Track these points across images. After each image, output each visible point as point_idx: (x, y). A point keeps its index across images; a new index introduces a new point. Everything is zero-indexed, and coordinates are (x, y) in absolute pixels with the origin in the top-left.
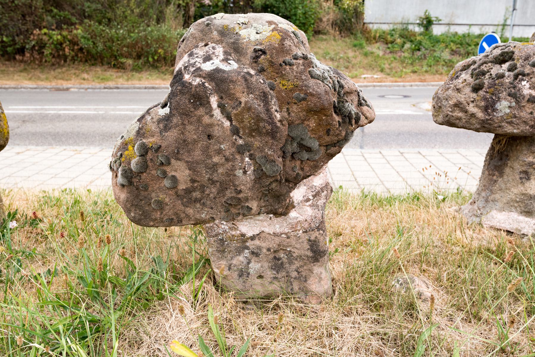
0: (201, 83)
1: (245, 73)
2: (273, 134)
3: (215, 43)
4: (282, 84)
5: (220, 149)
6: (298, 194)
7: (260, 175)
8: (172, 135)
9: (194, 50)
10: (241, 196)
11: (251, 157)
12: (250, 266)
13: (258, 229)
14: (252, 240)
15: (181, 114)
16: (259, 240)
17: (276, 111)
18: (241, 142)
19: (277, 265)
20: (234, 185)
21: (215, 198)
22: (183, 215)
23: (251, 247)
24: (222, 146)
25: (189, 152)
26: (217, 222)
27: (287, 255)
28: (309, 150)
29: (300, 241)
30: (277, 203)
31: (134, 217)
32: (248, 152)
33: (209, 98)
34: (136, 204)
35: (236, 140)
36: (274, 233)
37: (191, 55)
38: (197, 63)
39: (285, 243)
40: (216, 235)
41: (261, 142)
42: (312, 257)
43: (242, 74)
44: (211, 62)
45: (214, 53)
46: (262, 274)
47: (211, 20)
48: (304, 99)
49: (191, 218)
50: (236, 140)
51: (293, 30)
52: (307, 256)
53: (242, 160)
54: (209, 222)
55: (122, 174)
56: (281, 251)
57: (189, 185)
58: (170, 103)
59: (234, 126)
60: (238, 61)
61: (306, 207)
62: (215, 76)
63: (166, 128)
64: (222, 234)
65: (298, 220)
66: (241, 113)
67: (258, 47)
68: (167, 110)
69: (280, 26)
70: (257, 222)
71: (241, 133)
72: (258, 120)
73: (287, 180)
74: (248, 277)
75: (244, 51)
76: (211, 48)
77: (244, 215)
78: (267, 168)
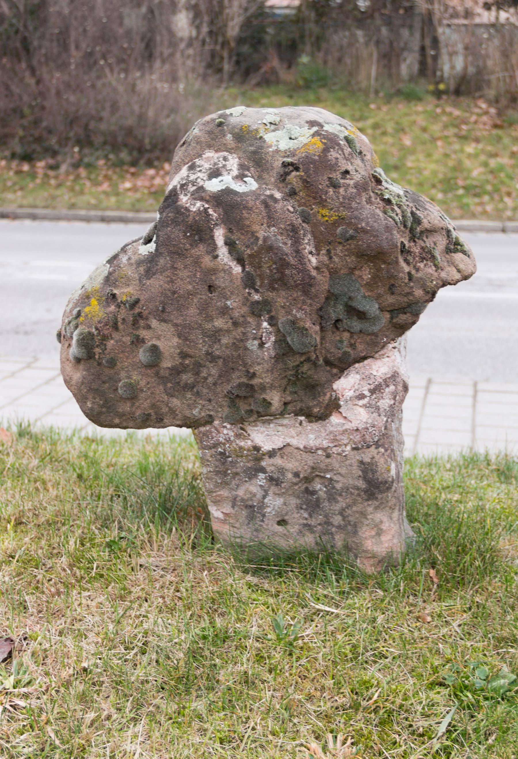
0: (202, 208)
1: (267, 196)
2: (306, 286)
3: (227, 151)
4: (325, 214)
5: (227, 307)
6: (347, 385)
7: (284, 350)
8: (157, 283)
9: (197, 160)
10: (255, 381)
11: (272, 321)
12: (266, 501)
13: (281, 439)
14: (270, 457)
15: (172, 253)
16: (282, 457)
17: (311, 253)
18: (257, 297)
19: (311, 503)
20: (245, 365)
21: (215, 384)
22: (165, 410)
23: (268, 469)
24: (229, 303)
25: (179, 310)
26: (216, 423)
27: (325, 487)
28: (362, 315)
29: (348, 462)
30: (312, 400)
31: (92, 409)
32: (268, 313)
33: (212, 230)
34: (96, 387)
35: (249, 294)
36: (305, 447)
37: (192, 168)
38: (199, 180)
39: (322, 466)
40: (215, 446)
41: (287, 298)
42: (366, 491)
43: (263, 197)
44: (220, 178)
45: (224, 166)
46: (286, 518)
47: (224, 116)
48: (352, 237)
49: (177, 415)
50: (249, 294)
51: (347, 133)
52: (358, 489)
53: (259, 326)
54: (204, 425)
55: (78, 341)
56: (317, 480)
57: (178, 361)
58: (157, 237)
59: (248, 273)
60: (259, 179)
61: (358, 408)
62: (225, 201)
63: (149, 273)
64: (224, 444)
65: (344, 428)
66: (258, 252)
67: (289, 160)
68: (152, 247)
69: (326, 127)
70: (280, 428)
71: (258, 284)
72: (282, 265)
73: (328, 362)
74: (263, 521)
75: (268, 165)
76: (221, 159)
77: (260, 415)
78: (293, 340)
